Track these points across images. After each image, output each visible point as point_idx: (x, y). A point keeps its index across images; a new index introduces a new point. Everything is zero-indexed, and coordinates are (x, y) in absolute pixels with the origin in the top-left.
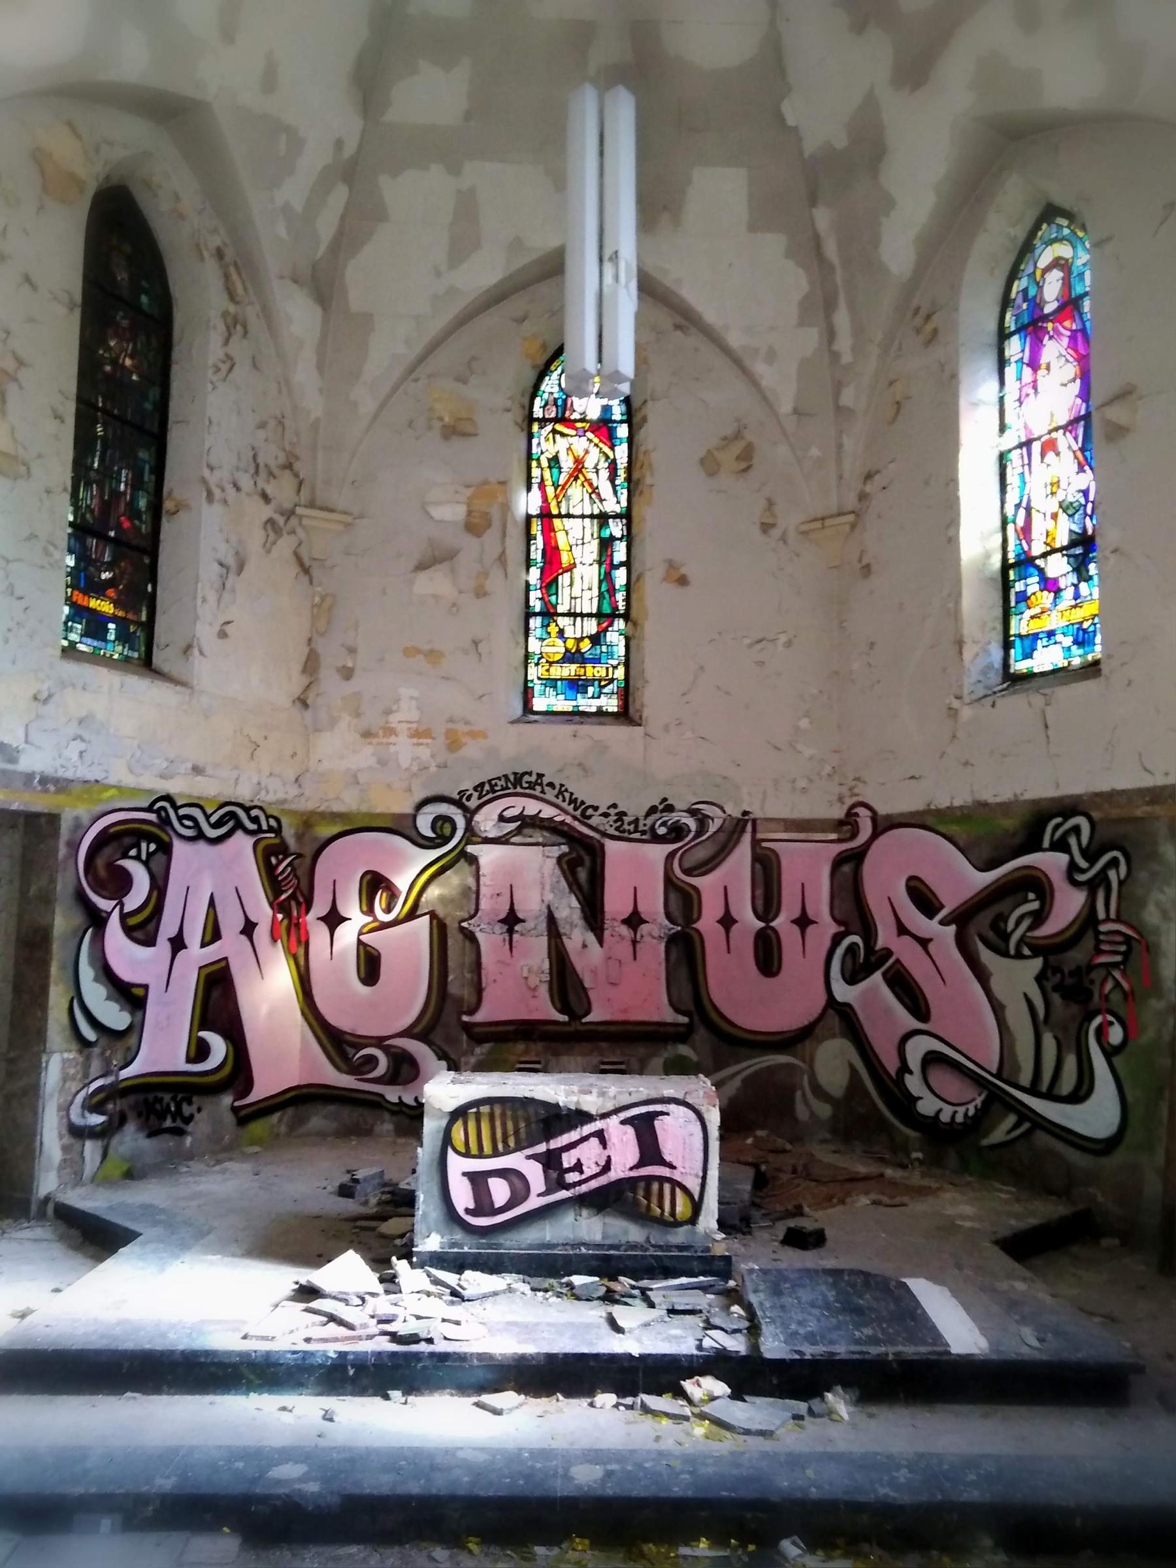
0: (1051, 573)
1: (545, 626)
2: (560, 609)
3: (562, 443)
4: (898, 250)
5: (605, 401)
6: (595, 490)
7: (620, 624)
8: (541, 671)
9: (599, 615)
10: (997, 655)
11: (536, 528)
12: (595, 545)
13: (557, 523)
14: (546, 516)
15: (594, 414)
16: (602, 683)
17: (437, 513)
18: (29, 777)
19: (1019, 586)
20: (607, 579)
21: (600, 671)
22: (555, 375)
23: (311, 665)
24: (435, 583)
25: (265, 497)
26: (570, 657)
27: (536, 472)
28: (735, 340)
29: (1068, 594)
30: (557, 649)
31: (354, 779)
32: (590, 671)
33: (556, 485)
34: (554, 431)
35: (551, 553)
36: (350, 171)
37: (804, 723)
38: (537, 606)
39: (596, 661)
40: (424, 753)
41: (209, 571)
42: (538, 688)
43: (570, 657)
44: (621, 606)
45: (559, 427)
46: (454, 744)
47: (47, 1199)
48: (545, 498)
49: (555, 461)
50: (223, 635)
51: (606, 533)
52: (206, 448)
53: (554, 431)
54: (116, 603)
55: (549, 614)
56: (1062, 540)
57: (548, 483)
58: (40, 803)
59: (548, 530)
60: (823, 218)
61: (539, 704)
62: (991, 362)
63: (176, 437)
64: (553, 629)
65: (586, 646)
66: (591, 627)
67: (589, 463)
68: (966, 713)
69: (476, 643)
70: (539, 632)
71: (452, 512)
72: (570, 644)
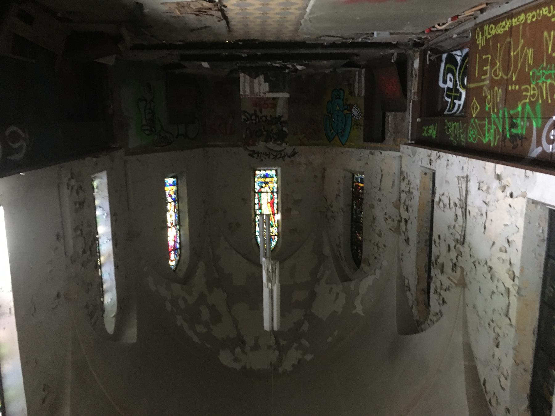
0: (170, 198)
4: (202, 266)
7: (256, 191)
9: (261, 192)
10: (179, 182)
12: (263, 208)
14: (274, 214)
18: (368, 149)
20: (259, 201)
23: (323, 177)
25: (333, 212)
26: (267, 183)
28: (234, 252)
30: (270, 185)
32: (262, 180)
35: (272, 206)
38: (275, 194)
39: (261, 182)
44: (256, 195)
46: (292, 161)
50: (339, 181)
51: (260, 211)
52: (482, 381)
54: (359, 186)
55: (272, 192)
58: (366, 144)
59: (273, 211)
62: (183, 243)
65: (264, 185)
66: (263, 190)
71: (294, 212)
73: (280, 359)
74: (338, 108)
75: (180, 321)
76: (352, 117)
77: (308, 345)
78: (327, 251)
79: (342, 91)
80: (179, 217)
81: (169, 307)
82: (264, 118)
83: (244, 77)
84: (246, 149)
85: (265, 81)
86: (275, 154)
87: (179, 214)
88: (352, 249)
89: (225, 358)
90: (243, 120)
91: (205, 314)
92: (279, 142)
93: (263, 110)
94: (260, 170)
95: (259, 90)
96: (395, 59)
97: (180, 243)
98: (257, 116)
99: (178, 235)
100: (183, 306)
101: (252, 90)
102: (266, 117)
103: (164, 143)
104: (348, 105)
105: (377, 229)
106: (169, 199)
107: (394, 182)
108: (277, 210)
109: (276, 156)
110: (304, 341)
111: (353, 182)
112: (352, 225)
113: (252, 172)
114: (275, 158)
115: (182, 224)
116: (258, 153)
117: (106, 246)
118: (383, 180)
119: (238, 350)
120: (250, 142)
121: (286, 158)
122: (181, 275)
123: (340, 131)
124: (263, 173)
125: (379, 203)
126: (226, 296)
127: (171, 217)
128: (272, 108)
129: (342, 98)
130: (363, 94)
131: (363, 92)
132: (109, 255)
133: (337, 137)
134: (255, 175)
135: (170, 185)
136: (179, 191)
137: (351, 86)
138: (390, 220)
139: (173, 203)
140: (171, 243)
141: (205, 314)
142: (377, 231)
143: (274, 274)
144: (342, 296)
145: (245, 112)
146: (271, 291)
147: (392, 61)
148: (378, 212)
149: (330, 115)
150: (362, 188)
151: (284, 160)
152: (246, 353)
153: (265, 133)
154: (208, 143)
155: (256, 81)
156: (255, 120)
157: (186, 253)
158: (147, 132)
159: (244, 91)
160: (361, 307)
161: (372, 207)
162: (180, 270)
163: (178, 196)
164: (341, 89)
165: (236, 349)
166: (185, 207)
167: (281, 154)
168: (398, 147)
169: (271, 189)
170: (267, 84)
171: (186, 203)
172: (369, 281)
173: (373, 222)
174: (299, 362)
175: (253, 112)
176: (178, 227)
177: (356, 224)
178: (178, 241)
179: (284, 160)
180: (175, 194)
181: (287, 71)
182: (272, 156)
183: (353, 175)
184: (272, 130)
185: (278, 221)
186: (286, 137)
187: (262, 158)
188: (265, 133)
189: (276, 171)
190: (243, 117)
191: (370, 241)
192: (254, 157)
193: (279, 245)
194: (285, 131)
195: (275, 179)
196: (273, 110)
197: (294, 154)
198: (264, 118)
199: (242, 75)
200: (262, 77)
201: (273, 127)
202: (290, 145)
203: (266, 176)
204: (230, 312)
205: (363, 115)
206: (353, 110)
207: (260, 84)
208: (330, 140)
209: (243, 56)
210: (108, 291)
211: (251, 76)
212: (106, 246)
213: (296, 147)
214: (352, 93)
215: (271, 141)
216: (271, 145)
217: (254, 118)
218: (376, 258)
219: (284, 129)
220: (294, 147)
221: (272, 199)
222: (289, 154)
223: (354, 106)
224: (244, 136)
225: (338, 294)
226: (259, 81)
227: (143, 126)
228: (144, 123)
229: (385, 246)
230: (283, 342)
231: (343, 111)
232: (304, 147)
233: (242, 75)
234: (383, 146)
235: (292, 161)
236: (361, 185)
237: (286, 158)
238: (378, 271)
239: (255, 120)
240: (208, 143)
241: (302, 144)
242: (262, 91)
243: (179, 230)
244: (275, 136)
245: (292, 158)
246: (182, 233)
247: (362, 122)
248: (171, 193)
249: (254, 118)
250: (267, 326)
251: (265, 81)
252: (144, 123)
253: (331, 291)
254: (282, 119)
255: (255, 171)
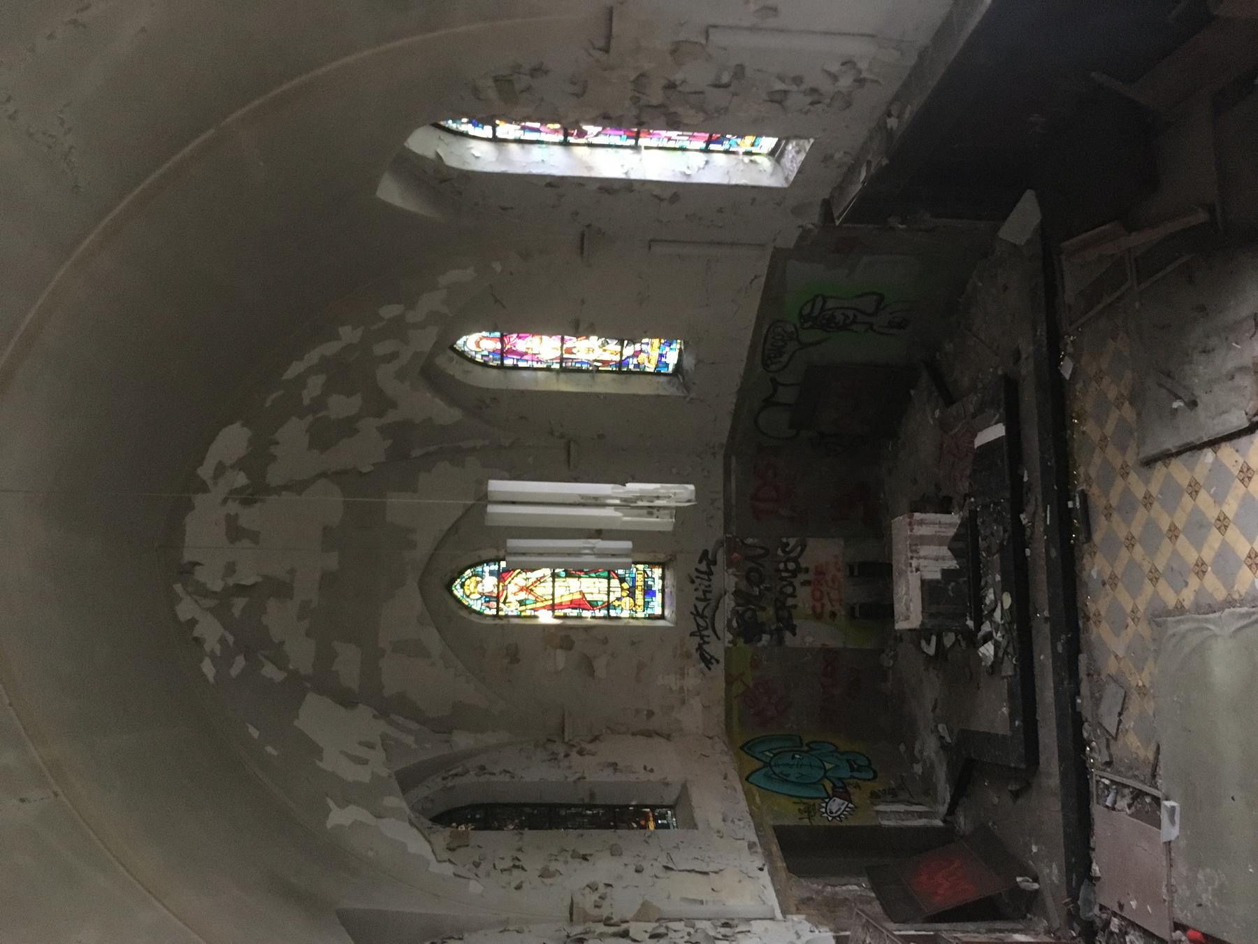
1: (615, 608)
2: (605, 599)
3: (511, 598)
5: (487, 574)
6: (538, 580)
8: (640, 610)
9: (609, 578)
10: (662, 379)
11: (559, 613)
13: (557, 601)
14: (553, 607)
15: (494, 580)
16: (646, 576)
17: (561, 666)
19: (631, 367)
21: (640, 578)
22: (471, 603)
23: (649, 734)
24: (600, 665)
26: (632, 594)
27: (528, 613)
29: (644, 347)
30: (627, 602)
31: (706, 708)
32: (640, 583)
33: (536, 602)
34: (504, 602)
35: (574, 604)
36: (383, 711)
37: (674, 470)
38: (603, 613)
39: (634, 579)
40: (692, 671)
41: (618, 777)
42: (649, 611)
43: (632, 594)
45: (502, 600)
46: (688, 655)
47: (944, 821)
48: (544, 607)
49: (522, 603)
53: (504, 602)
55: (608, 606)
56: (618, 348)
57: (534, 606)
59: (561, 606)
60: (416, 453)
61: (658, 611)
62: (514, 373)
63: (548, 799)
64: (616, 603)
65: (625, 586)
66: (615, 582)
67: (523, 583)
68: (693, 395)
69: (633, 643)
70: (618, 611)
72: (625, 594)
73: (202, 592)
74: (828, 766)
75: (349, 334)
76: (823, 799)
77: (234, 672)
78: (463, 740)
79: (871, 775)
80: (580, 370)
81: (390, 311)
82: (789, 590)
83: (951, 525)
84: (720, 544)
85: (945, 572)
86: (707, 613)
87: (587, 371)
88: (474, 807)
89: (232, 441)
90: (784, 540)
91: (341, 406)
92: (735, 624)
93: (808, 589)
94: (663, 578)
95: (925, 558)
96: (1024, 885)
97: (515, 367)
98: (794, 574)
99: (536, 365)
100: (380, 349)
101: (923, 540)
102: (793, 595)
103: (770, 346)
104: (844, 787)
105: (559, 866)
106: (629, 351)
107: (702, 902)
108: (565, 617)
109: (702, 616)
110: (240, 662)
111: (653, 808)
112: (541, 805)
113: (661, 557)
114: (697, 614)
115: (562, 376)
116: (710, 573)
117: (609, 157)
118: (693, 874)
119: (241, 479)
120: (736, 555)
121: (697, 640)
122: (441, 361)
123: (777, 770)
124: (657, 586)
125: (632, 868)
126: (364, 470)
127: (590, 350)
128: (814, 608)
129: (856, 774)
130: (885, 823)
131: (892, 823)
132: (590, 168)
133: (761, 764)
134: (652, 564)
135: (661, 356)
136: (642, 377)
137: (893, 795)
138: (595, 897)
139: (617, 358)
140: (521, 344)
141: (341, 406)
142: (553, 866)
143: (645, 511)
144: (363, 775)
145: (804, 547)
146: (597, 502)
147: (1019, 879)
148: (603, 868)
149: (805, 748)
150: (645, 827)
151: (692, 634)
152: (225, 501)
153: (756, 591)
154: (734, 459)
155: (944, 551)
156: (786, 570)
157: (491, 380)
158: (806, 311)
159: (921, 523)
160: (348, 823)
161: (615, 852)
162: (451, 359)
163: (629, 372)
164: (875, 777)
165: (242, 474)
166: (606, 386)
167: (706, 628)
168: (793, 909)
169: (616, 603)
170: (938, 576)
171: (613, 391)
172: (416, 844)
173: (575, 855)
174: (196, 639)
175: (803, 565)
176: (557, 366)
177: (544, 815)
178: (521, 364)
179: (692, 634)
180: (637, 365)
181: (970, 623)
182: (701, 605)
183: (670, 807)
184: (764, 609)
185: (535, 617)
186: (746, 642)
187: (697, 581)
188: (756, 591)
189: (662, 617)
190: (792, 541)
191: (520, 850)
192: (700, 562)
193: (474, 618)
194: (760, 640)
195: (640, 614)
196: (809, 612)
197: (707, 660)
198: (789, 590)
199: (954, 518)
200: (953, 564)
201: (771, 611)
202: (727, 650)
203: (648, 592)
204: (323, 475)
205: (836, 823)
206: (838, 800)
207: (937, 559)
208: (747, 748)
209: (1022, 516)
210: (500, 152)
211: (956, 538)
212: (609, 157)
213: (722, 665)
214: (875, 796)
215: (738, 605)
216: (729, 603)
217: (791, 566)
218: (477, 865)
219: (766, 638)
220: (722, 660)
221: (592, 605)
222: (705, 647)
223: (850, 802)
224: (750, 541)
225: (365, 762)
226: (943, 558)
227: (825, 299)
228: (830, 304)
229: (518, 888)
230: (239, 603)
231: (825, 776)
232: (723, 685)
233: (954, 518)
234: (783, 875)
235: (688, 655)
236: (652, 825)
237: (697, 640)
238: (448, 869)
239: (786, 570)
240: (734, 459)
241: (729, 681)
242: (923, 562)
243: (548, 369)
244: (749, 614)
245: (697, 656)
246: (540, 373)
247: (817, 821)
248: (642, 357)
249: (791, 566)
250: (498, 486)
251: (945, 572)
252: (830, 304)
253: (371, 746)
254: (788, 634)
255: (663, 565)
